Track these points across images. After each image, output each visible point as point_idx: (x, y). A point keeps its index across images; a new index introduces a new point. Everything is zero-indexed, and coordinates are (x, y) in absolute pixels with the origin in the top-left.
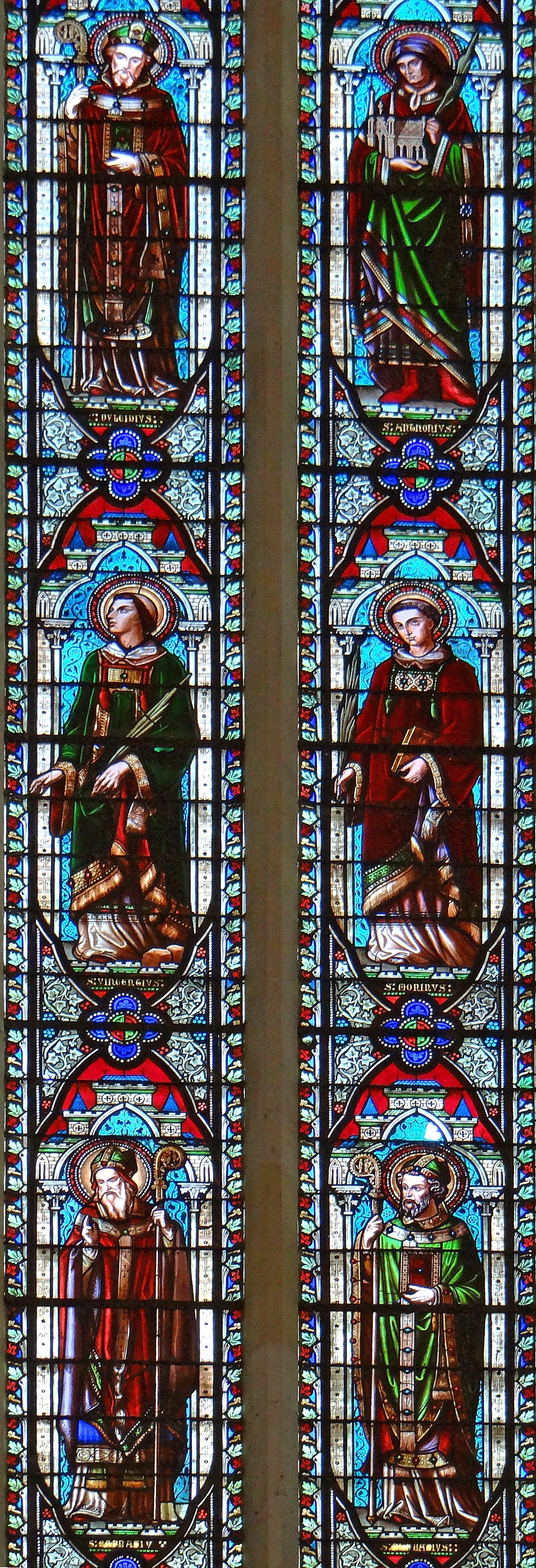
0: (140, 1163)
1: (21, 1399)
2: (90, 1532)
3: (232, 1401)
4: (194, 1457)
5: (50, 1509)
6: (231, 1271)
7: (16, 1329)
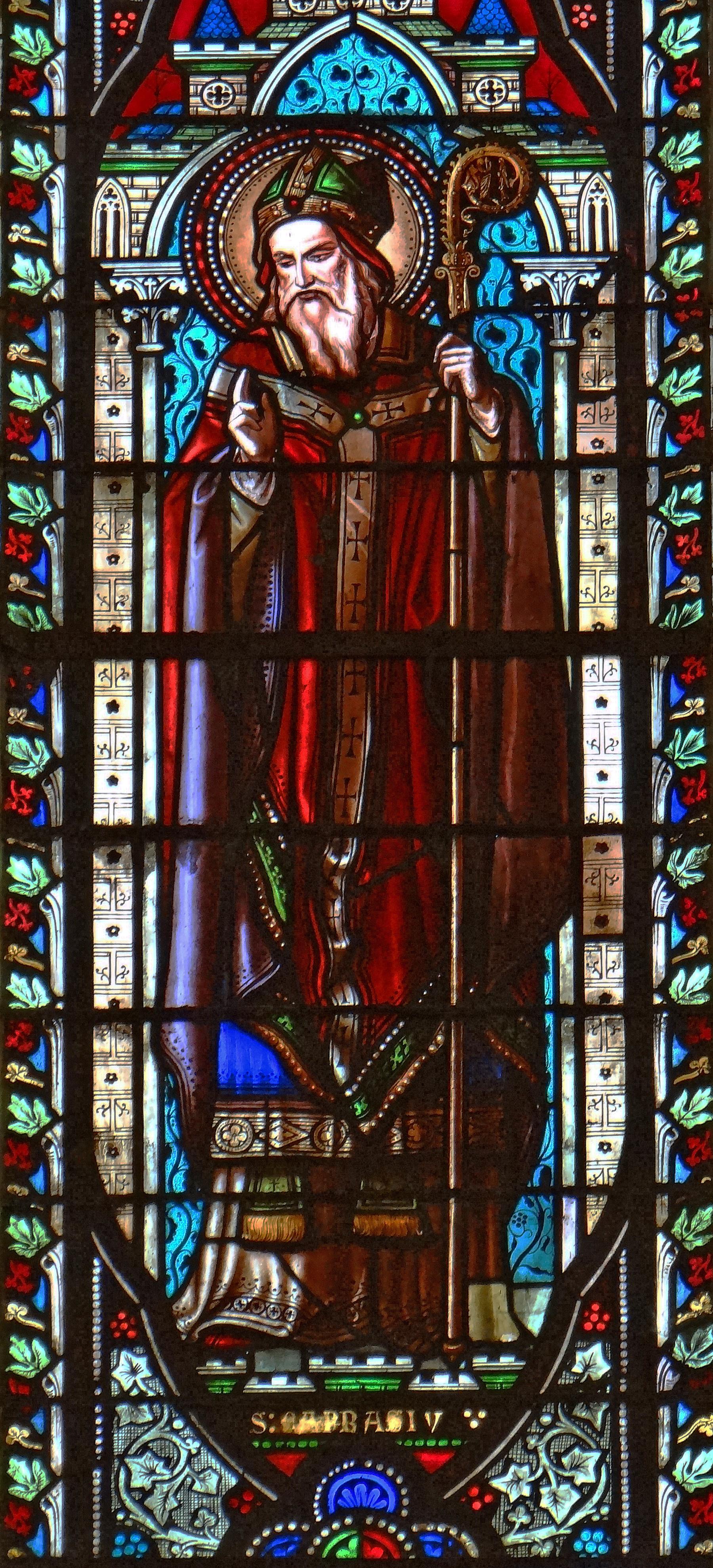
0: (400, 199)
1: (45, 958)
2: (254, 1386)
3: (682, 947)
4: (569, 1133)
5: (133, 1311)
6: (674, 531)
7: (31, 735)
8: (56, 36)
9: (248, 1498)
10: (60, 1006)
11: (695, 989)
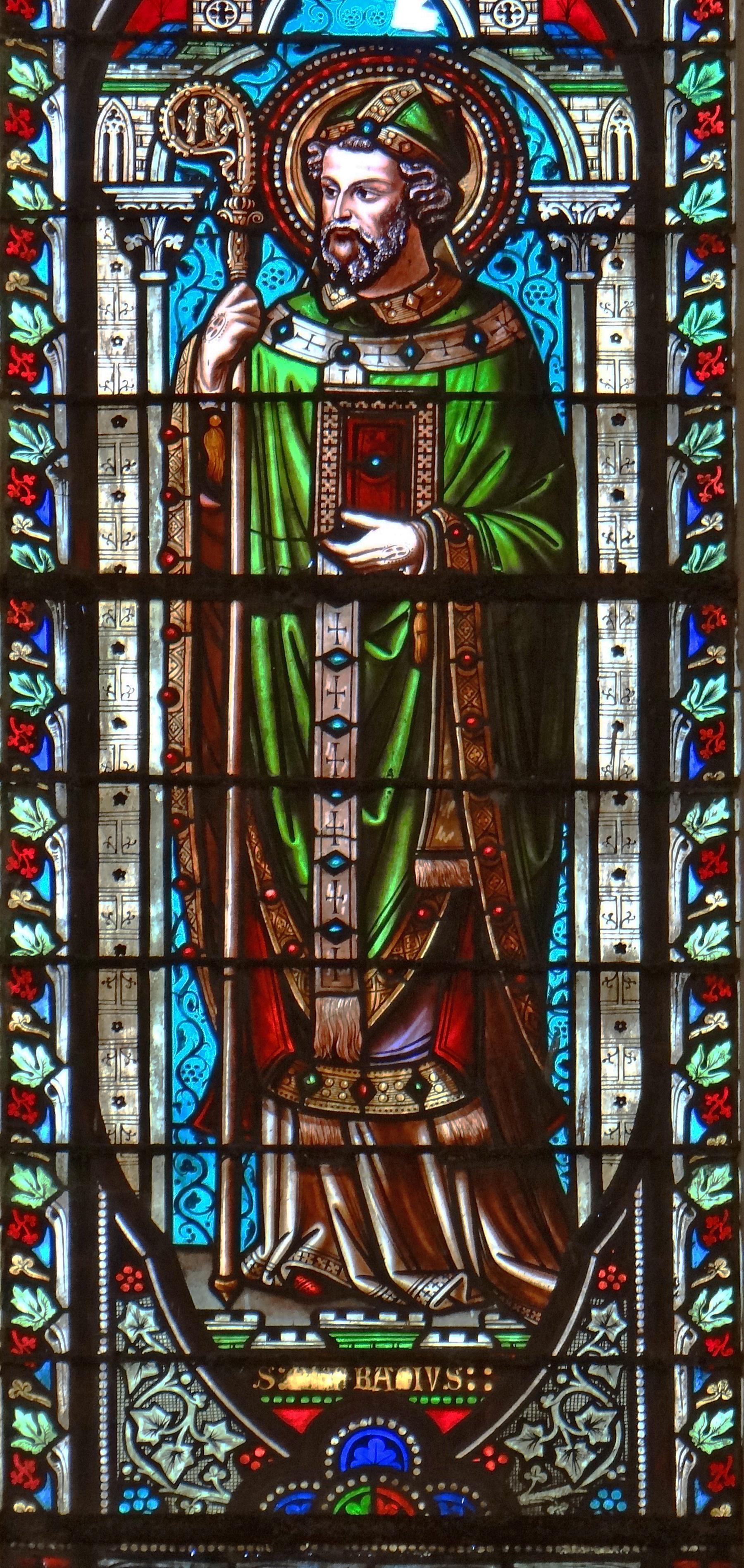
7: (32, 671)
8: (57, 682)
9: (259, 1452)
10: (64, 952)
11: (714, 943)
